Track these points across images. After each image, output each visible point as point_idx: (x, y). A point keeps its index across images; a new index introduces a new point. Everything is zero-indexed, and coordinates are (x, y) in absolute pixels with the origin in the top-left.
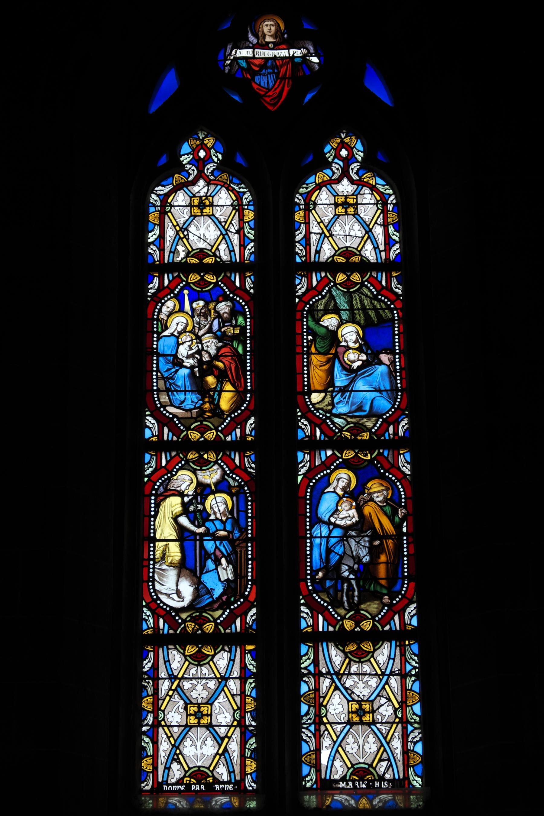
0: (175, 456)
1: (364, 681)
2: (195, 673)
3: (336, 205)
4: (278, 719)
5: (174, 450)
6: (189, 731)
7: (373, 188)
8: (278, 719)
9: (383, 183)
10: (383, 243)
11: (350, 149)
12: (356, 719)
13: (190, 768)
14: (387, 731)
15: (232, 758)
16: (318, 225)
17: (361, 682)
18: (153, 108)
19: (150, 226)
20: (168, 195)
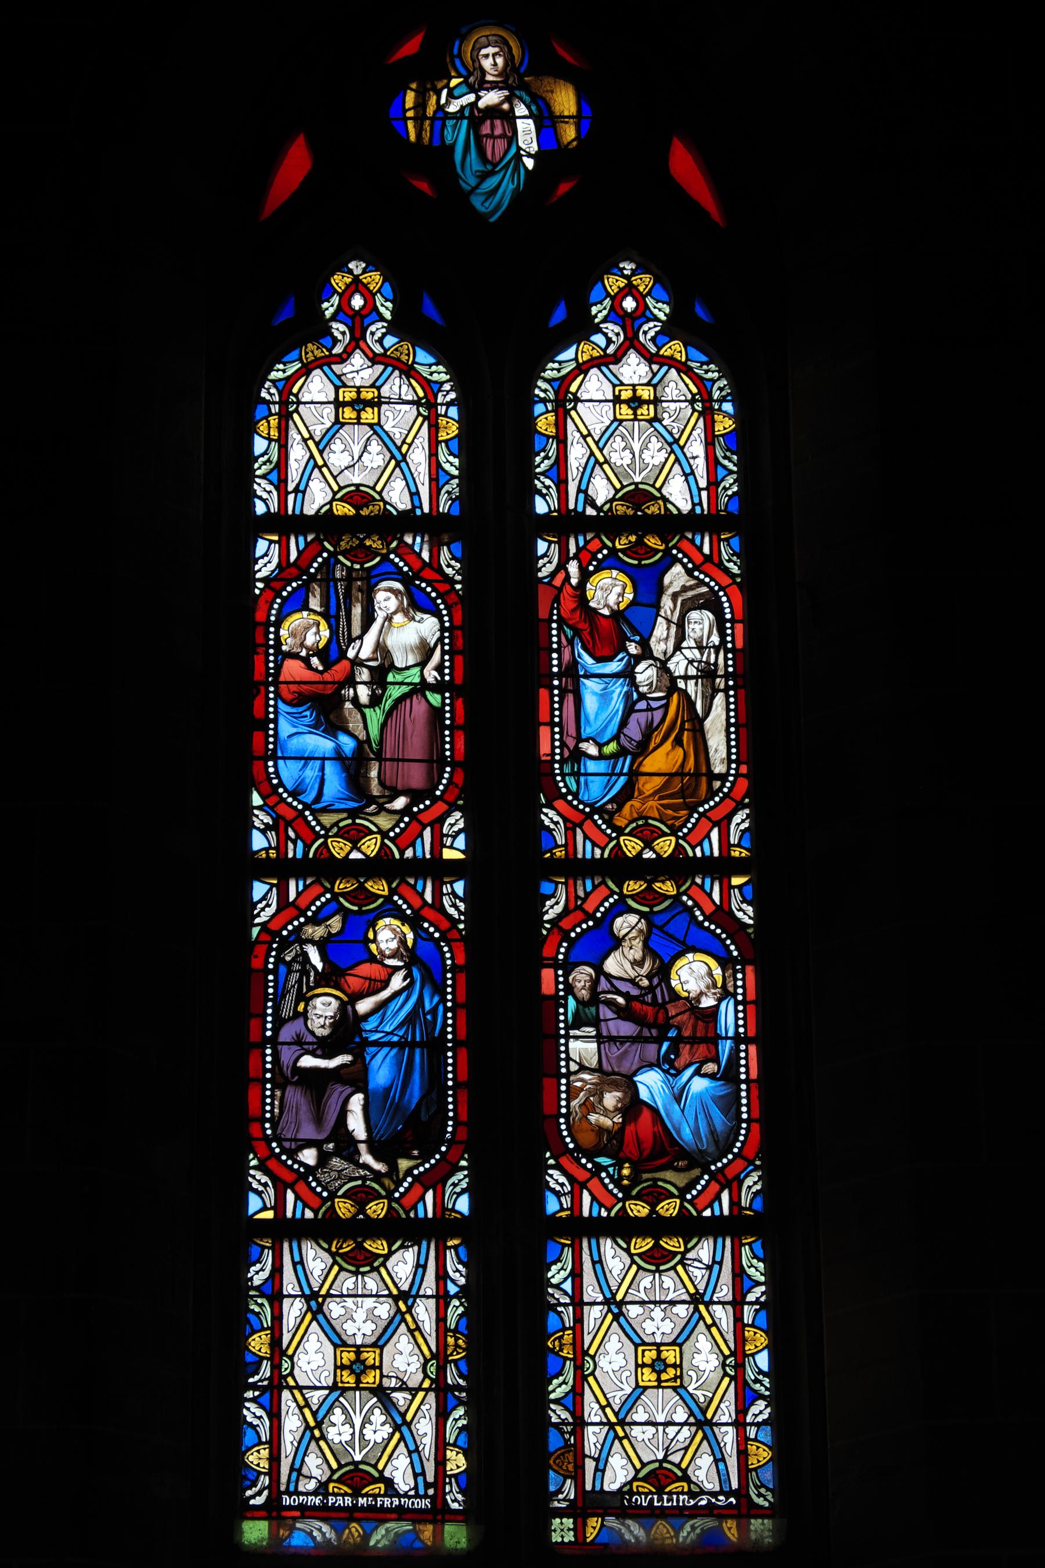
2: (352, 1286)
3: (338, 404)
4: (507, 1363)
8: (507, 1363)
12: (349, 1379)
13: (644, 1465)
14: (708, 1399)
15: (722, 1445)
16: (582, 440)
20: (291, 380)
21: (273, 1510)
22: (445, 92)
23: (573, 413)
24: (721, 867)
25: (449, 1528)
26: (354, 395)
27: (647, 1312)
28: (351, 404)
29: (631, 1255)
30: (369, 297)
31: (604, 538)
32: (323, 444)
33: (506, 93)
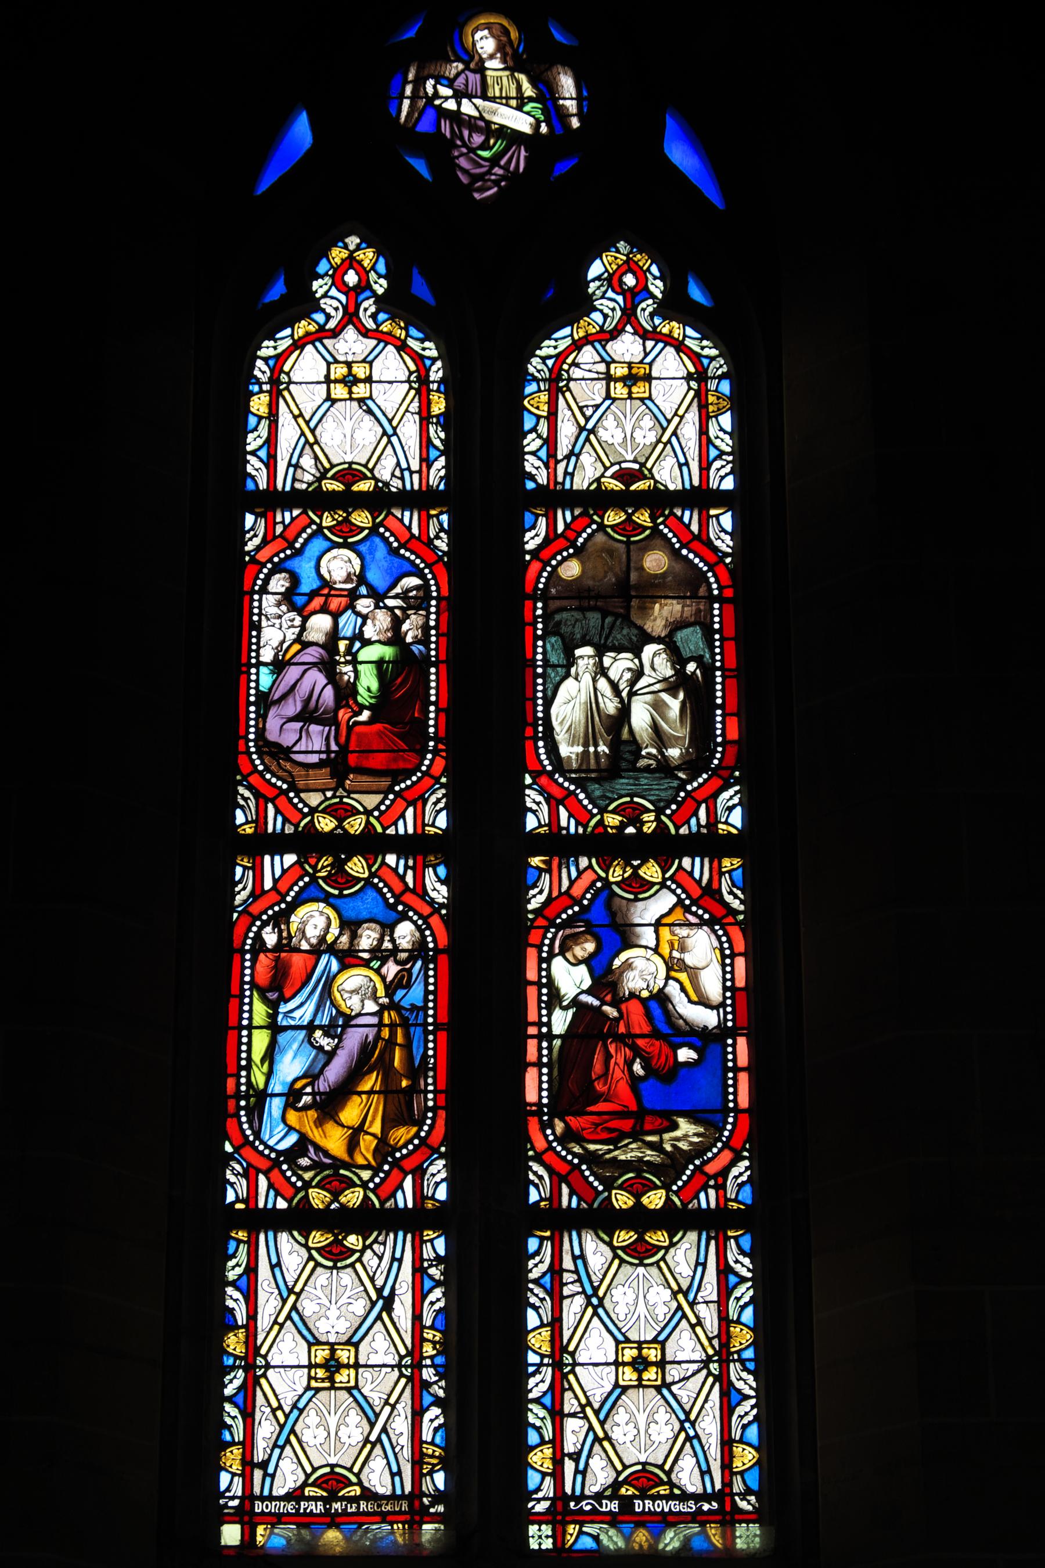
1: (339, 1304)
4: (483, 1368)
5: (297, 507)
6: (314, 1396)
8: (483, 1368)
11: (641, 275)
17: (333, 1307)
18: (263, 188)
19: (252, 421)
21: (562, 1511)
25: (740, 1530)
26: (625, 371)
29: (613, 1249)
30: (640, 273)
31: (311, 514)
32: (605, 1411)
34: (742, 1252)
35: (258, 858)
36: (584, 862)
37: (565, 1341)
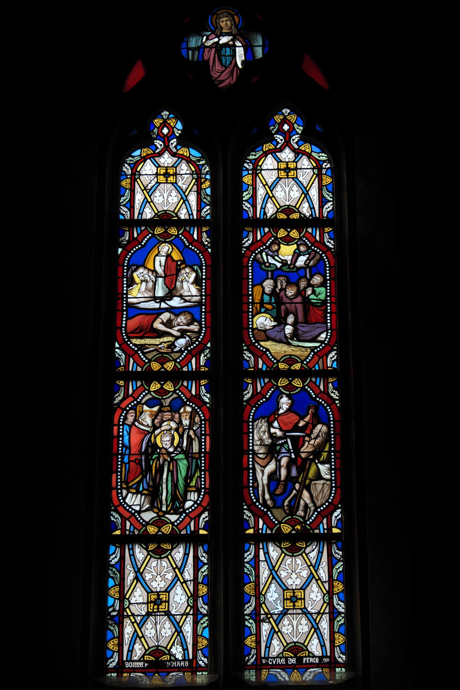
0: (144, 230)
1: (296, 572)
4: (227, 600)
6: (158, 186)
7: (309, 156)
8: (227, 600)
9: (318, 150)
10: (328, 639)
15: (186, 637)
21: (259, 666)
22: (205, 38)
23: (260, 175)
24: (195, 376)
26: (285, 166)
27: (289, 575)
28: (284, 170)
32: (272, 187)
33: (231, 37)
34: (342, 653)
35: (127, 382)
36: (267, 230)
37: (328, 607)
